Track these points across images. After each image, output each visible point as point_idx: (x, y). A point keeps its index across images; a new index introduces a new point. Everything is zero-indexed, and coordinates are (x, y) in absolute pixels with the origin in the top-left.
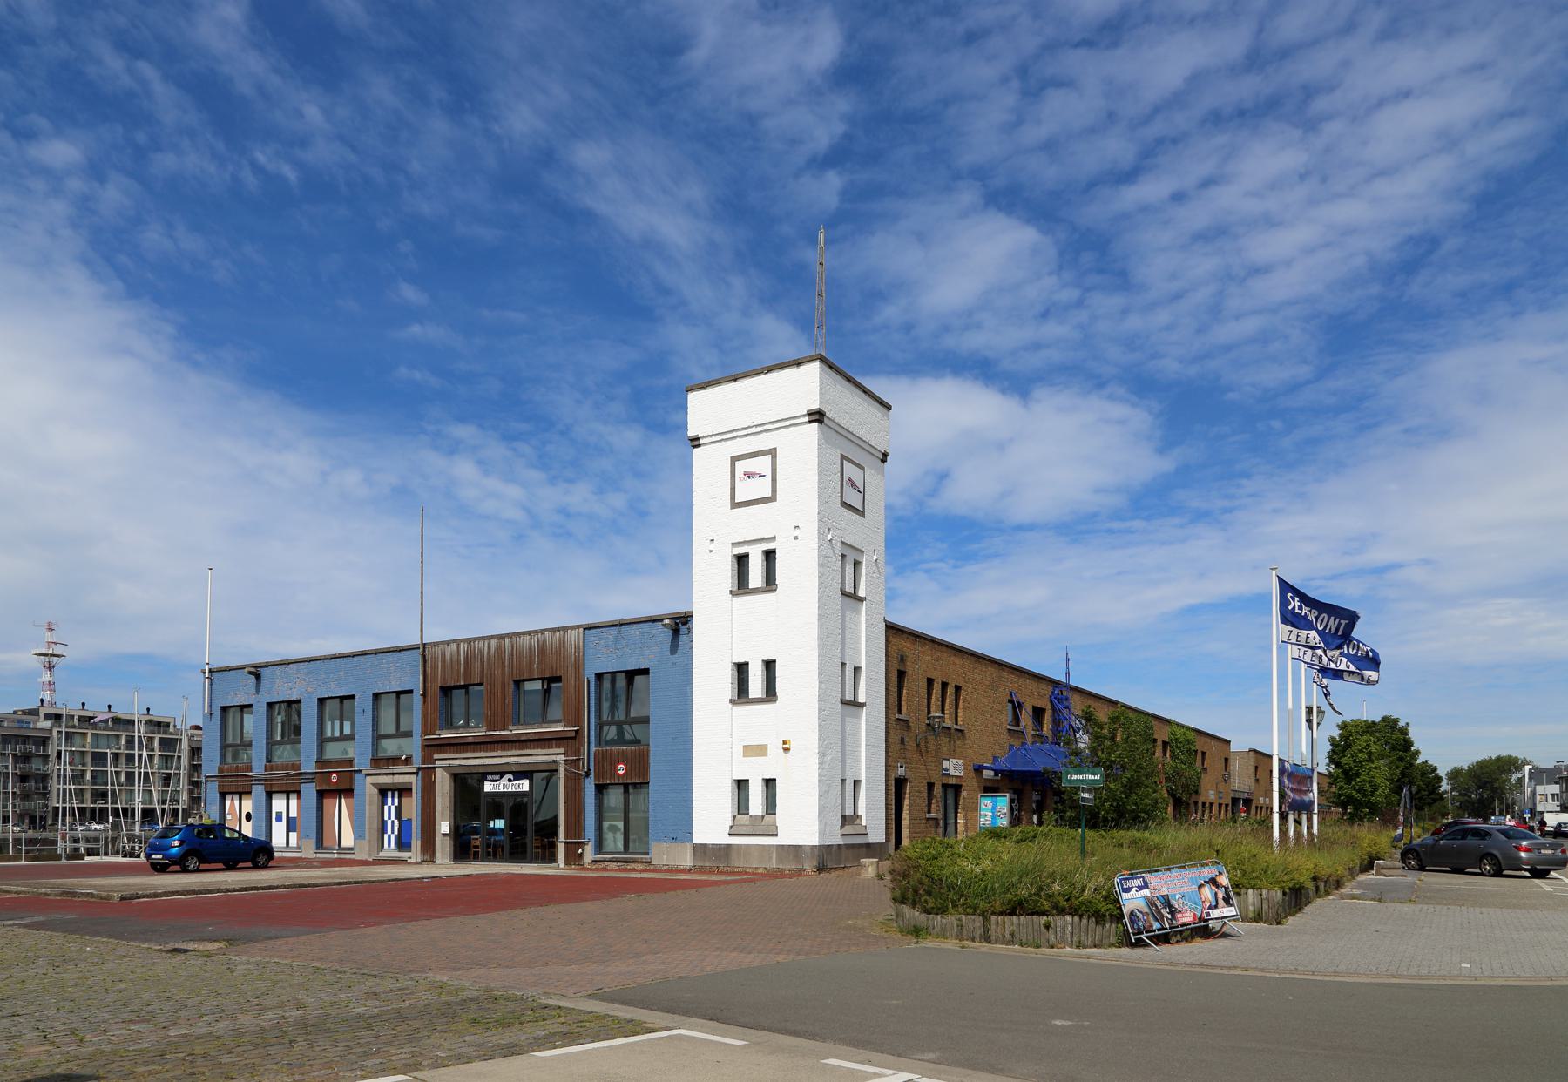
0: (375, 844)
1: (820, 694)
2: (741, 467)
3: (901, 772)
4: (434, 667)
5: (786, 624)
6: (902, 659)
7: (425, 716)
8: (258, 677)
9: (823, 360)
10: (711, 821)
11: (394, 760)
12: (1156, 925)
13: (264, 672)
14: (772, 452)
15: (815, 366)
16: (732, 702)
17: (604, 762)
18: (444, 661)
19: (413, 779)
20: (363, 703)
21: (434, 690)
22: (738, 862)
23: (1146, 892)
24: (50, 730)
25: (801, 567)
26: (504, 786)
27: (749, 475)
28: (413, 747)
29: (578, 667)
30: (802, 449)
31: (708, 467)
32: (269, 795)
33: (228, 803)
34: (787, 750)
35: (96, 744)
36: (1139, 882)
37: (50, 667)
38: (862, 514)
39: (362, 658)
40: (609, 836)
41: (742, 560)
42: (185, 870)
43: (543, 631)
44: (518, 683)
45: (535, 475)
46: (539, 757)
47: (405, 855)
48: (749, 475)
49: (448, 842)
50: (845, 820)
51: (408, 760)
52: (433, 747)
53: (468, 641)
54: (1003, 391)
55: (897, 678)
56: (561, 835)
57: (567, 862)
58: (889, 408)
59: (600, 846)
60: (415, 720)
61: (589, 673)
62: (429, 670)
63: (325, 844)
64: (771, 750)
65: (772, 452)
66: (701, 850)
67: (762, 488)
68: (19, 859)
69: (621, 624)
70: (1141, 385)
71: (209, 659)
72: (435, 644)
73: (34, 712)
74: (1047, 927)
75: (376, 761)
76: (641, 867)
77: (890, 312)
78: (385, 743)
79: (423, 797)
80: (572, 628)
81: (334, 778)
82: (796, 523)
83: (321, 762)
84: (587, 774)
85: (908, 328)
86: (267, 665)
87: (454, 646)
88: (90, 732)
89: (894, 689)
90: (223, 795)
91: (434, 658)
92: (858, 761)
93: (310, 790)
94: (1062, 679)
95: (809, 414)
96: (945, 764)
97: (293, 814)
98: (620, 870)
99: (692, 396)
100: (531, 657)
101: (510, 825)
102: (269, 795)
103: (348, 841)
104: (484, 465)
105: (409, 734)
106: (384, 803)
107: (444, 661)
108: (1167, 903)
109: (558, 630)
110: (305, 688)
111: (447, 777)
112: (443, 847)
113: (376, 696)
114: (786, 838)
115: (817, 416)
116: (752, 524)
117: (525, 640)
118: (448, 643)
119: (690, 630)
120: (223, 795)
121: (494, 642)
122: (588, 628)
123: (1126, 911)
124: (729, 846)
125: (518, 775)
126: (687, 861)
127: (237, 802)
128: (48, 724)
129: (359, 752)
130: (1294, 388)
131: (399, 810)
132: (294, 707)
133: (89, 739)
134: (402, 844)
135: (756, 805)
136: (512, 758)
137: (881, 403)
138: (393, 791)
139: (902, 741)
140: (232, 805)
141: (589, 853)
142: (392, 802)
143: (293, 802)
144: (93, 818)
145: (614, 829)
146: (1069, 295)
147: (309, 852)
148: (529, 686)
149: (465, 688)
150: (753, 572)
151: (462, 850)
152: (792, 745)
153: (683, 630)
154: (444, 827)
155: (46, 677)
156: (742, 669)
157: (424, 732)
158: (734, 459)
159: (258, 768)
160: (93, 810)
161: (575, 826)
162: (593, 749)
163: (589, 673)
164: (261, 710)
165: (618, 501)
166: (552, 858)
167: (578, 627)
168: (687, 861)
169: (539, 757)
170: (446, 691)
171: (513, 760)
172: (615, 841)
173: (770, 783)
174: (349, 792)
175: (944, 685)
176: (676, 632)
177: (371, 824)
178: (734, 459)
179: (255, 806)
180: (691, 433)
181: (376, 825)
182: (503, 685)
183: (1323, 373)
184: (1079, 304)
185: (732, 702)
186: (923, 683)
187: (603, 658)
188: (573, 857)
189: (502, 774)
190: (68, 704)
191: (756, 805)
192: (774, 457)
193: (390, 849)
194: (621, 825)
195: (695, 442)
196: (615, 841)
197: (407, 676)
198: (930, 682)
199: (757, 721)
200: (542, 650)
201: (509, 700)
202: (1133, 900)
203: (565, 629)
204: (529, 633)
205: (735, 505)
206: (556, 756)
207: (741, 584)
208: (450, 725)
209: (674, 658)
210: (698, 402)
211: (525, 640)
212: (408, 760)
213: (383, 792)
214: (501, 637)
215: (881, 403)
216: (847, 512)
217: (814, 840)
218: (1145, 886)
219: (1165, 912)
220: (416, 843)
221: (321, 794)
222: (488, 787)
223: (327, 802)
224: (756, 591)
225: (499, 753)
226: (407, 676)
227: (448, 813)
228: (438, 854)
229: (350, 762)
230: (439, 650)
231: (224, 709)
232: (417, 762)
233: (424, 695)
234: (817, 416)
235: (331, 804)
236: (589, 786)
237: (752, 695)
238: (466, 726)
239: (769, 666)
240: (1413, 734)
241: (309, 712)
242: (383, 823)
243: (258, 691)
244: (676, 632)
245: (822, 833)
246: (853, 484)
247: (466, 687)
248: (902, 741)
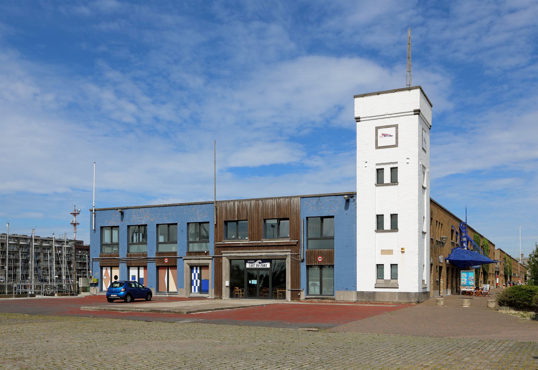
0: (189, 290)
2: (380, 132)
4: (221, 212)
7: (216, 233)
8: (122, 213)
10: (366, 281)
14: (396, 126)
16: (376, 231)
17: (311, 255)
18: (226, 209)
19: (210, 262)
20: (182, 227)
22: (378, 299)
25: (409, 175)
26: (256, 265)
27: (385, 135)
28: (210, 247)
29: (297, 214)
33: (104, 271)
34: (403, 252)
39: (181, 207)
40: (311, 289)
41: (380, 171)
42: (126, 302)
43: (279, 198)
44: (265, 220)
45: (144, 99)
46: (277, 253)
48: (385, 135)
49: (228, 290)
52: (219, 248)
53: (239, 201)
54: (382, 66)
56: (288, 286)
57: (292, 298)
61: (303, 217)
62: (218, 214)
63: (160, 290)
65: (396, 126)
66: (361, 294)
68: (12, 296)
69: (320, 196)
70: (448, 65)
71: (94, 205)
75: (189, 253)
76: (330, 301)
77: (332, 23)
79: (215, 270)
81: (166, 261)
83: (158, 253)
84: (303, 261)
85: (338, 33)
87: (232, 203)
90: (102, 268)
91: (221, 208)
93: (152, 266)
95: (414, 111)
98: (331, 303)
99: (357, 100)
102: (128, 268)
103: (173, 288)
104: (119, 94)
106: (192, 271)
107: (226, 209)
109: (287, 197)
110: (150, 220)
111: (228, 261)
112: (226, 292)
113: (188, 224)
114: (402, 289)
115: (417, 112)
116: (386, 157)
117: (269, 202)
118: (229, 201)
119: (355, 201)
120: (102, 268)
121: (253, 202)
124: (374, 293)
125: (264, 261)
126: (354, 298)
127: (109, 271)
130: (516, 68)
132: (142, 228)
134: (201, 290)
136: (264, 253)
138: (197, 267)
140: (107, 272)
141: (303, 295)
142: (196, 272)
143: (142, 271)
145: (314, 285)
146: (420, 19)
147: (183, 294)
152: (405, 250)
157: (216, 241)
158: (377, 128)
159: (123, 255)
164: (123, 229)
165: (186, 113)
166: (284, 297)
167: (298, 197)
168: (354, 298)
169: (277, 253)
171: (263, 254)
173: (394, 266)
174: (174, 267)
176: (348, 201)
177: (187, 282)
178: (377, 128)
179: (121, 274)
180: (356, 115)
181: (189, 282)
182: (258, 221)
183: (533, 62)
184: (422, 25)
185: (375, 231)
187: (310, 210)
188: (295, 295)
189: (256, 260)
193: (195, 292)
194: (318, 283)
195: (358, 119)
199: (388, 239)
200: (279, 206)
203: (291, 197)
204: (272, 198)
205: (377, 147)
206: (287, 253)
207: (380, 181)
208: (226, 237)
209: (346, 212)
212: (207, 254)
213: (192, 267)
214: (257, 200)
217: (417, 291)
220: (211, 290)
221: (158, 268)
222: (248, 266)
223: (161, 271)
224: (387, 185)
225: (256, 251)
227: (228, 277)
228: (223, 295)
232: (212, 254)
234: (417, 112)
235: (163, 273)
236: (303, 266)
238: (237, 238)
239: (394, 217)
241: (151, 231)
243: (122, 219)
244: (348, 201)
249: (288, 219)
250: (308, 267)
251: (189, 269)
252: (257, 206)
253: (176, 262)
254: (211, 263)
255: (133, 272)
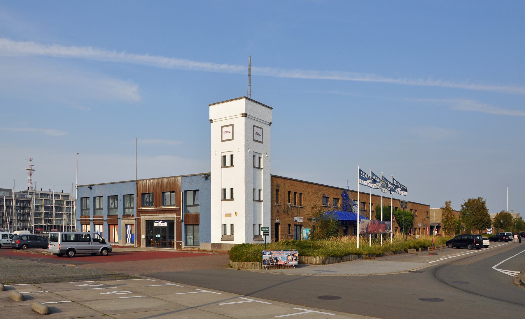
1: (245, 199)
2: (224, 129)
3: (277, 221)
4: (140, 187)
5: (235, 178)
6: (278, 186)
8: (91, 188)
9: (246, 98)
10: (216, 237)
11: (129, 216)
12: (271, 263)
13: (93, 187)
14: (232, 125)
15: (243, 100)
20: (120, 198)
21: (140, 195)
23: (270, 256)
24: (31, 198)
27: (226, 132)
28: (134, 212)
29: (180, 189)
30: (240, 124)
31: (215, 128)
32: (95, 225)
35: (46, 203)
36: (269, 253)
37: (31, 174)
38: (262, 142)
43: (170, 177)
44: (163, 193)
47: (132, 245)
48: (226, 132)
50: (255, 237)
51: (133, 216)
52: (140, 212)
53: (149, 180)
55: (275, 191)
58: (272, 108)
59: (186, 244)
60: (134, 204)
64: (231, 217)
65: (232, 125)
66: (214, 245)
67: (229, 136)
71: (77, 183)
72: (140, 180)
73: (26, 192)
74: (253, 264)
78: (127, 210)
80: (178, 176)
82: (238, 148)
83: (109, 216)
84: (182, 221)
86: (93, 185)
88: (44, 199)
89: (275, 196)
90: (82, 225)
91: (140, 185)
92: (260, 218)
93: (106, 224)
94: (346, 188)
95: (242, 114)
96: (295, 218)
97: (101, 231)
99: (211, 108)
100: (167, 186)
101: (162, 236)
102: (95, 225)
103: (117, 240)
105: (133, 208)
106: (127, 228)
108: (276, 259)
109: (174, 177)
118: (144, 180)
120: (82, 225)
121: (156, 180)
122: (182, 177)
123: (263, 260)
126: (210, 248)
128: (30, 196)
129: (119, 213)
131: (131, 231)
133: (43, 201)
134: (132, 242)
135: (228, 232)
136: (162, 216)
137: (269, 107)
139: (278, 212)
144: (45, 230)
145: (190, 238)
148: (166, 194)
149: (150, 195)
150: (227, 162)
151: (148, 243)
153: (209, 178)
154: (143, 237)
155: (29, 178)
156: (225, 190)
157: (137, 208)
159: (91, 218)
160: (45, 226)
161: (179, 238)
162: (184, 213)
163: (183, 191)
170: (143, 195)
172: (190, 242)
175: (295, 193)
178: (222, 127)
180: (210, 119)
181: (124, 235)
185: (222, 200)
186: (285, 193)
189: (159, 221)
190: (37, 189)
191: (228, 232)
192: (233, 127)
193: (129, 243)
194: (192, 237)
195: (211, 121)
196: (190, 242)
197: (132, 190)
198: (289, 192)
201: (161, 198)
202: (266, 257)
203: (176, 177)
204: (166, 178)
205: (222, 141)
207: (224, 165)
210: (213, 109)
211: (165, 180)
213: (126, 225)
215: (269, 107)
216: (256, 143)
218: (271, 254)
219: (275, 261)
220: (135, 241)
221: (109, 225)
222: (155, 224)
223: (188, 227)
226: (132, 190)
229: (117, 216)
230: (141, 182)
231: (82, 198)
233: (137, 196)
236: (183, 225)
237: (227, 199)
240: (487, 205)
242: (127, 235)
245: (246, 240)
246: (258, 134)
247: (149, 194)
248: (278, 212)
249: (174, 192)
250: (186, 225)
251: (124, 227)
252: (158, 182)
253: (117, 221)
254: (134, 222)
255: (97, 227)
